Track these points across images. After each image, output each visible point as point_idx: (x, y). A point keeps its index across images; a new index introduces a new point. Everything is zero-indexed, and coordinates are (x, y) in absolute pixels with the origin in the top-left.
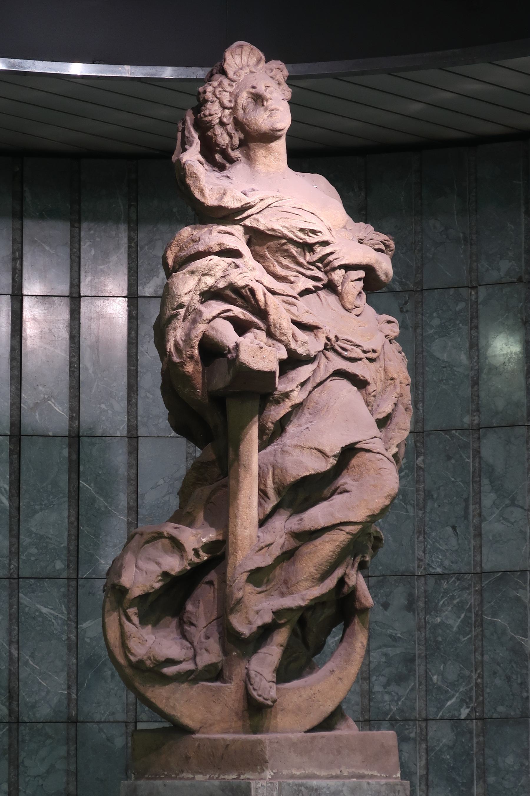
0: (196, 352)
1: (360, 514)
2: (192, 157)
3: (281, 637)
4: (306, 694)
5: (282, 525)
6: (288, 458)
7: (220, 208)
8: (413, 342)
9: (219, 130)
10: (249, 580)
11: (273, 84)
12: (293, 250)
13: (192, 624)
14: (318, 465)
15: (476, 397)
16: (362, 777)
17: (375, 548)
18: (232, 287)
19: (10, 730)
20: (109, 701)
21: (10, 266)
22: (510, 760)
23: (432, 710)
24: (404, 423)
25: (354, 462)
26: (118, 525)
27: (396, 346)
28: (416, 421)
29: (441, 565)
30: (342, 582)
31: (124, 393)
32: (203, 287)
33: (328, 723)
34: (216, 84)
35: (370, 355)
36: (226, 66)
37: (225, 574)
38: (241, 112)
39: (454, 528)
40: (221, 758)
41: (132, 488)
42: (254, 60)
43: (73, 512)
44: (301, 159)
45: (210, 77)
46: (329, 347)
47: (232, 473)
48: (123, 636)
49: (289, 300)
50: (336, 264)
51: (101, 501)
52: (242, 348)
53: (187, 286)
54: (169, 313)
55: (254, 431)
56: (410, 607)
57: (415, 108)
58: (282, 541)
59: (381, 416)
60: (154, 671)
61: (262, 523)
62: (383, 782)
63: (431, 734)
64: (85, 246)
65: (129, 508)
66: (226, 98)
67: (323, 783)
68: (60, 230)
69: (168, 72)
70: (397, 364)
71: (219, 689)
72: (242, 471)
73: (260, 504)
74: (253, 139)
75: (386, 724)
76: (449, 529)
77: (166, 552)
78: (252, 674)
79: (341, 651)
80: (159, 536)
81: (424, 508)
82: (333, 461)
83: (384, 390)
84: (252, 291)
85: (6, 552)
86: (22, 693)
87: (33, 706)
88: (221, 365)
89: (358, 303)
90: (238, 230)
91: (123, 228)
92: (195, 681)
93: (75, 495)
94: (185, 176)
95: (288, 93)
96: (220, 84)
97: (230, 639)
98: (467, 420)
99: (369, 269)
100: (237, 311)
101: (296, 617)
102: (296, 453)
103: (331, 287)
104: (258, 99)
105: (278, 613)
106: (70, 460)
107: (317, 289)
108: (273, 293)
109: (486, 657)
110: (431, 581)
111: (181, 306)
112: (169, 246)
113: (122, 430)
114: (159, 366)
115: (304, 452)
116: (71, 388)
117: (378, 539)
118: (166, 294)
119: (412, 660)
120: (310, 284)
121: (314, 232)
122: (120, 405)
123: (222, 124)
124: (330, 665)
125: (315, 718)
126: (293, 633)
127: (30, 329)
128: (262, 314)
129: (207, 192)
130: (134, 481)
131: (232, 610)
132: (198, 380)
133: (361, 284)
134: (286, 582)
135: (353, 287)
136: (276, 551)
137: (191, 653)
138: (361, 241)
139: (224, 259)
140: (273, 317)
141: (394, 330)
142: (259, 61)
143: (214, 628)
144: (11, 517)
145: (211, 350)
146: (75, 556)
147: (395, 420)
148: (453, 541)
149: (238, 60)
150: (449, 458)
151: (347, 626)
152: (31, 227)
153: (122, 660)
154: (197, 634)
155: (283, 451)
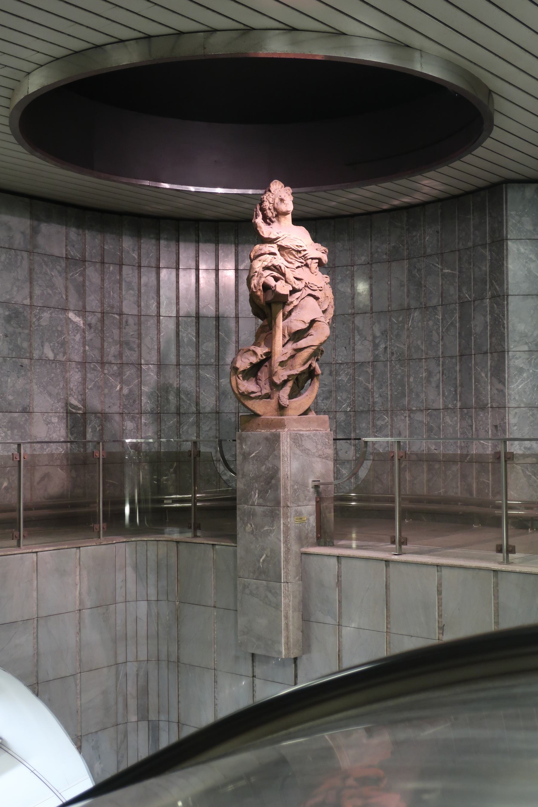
0: (261, 288)
1: (317, 343)
2: (259, 221)
3: (290, 384)
4: (299, 403)
5: (291, 346)
6: (292, 324)
7: (269, 238)
8: (333, 284)
9: (268, 211)
10: (279, 365)
11: (287, 195)
12: (294, 253)
13: (260, 380)
14: (304, 326)
15: (353, 303)
16: (317, 430)
17: (321, 354)
18: (273, 266)
19: (197, 416)
20: (230, 406)
21: (195, 259)
22: (364, 425)
23: (338, 409)
24: (331, 312)
25: (315, 325)
26: (232, 347)
27: (329, 286)
28: (335, 311)
29: (341, 360)
30: (310, 365)
31: (234, 302)
32: (264, 266)
33: (305, 413)
34: (267, 195)
35: (320, 289)
36: (271, 189)
37: (271, 363)
38: (276, 205)
39: (345, 348)
40: (270, 424)
41: (237, 335)
42: (280, 187)
43: (217, 343)
44: (296, 221)
45: (265, 193)
46: (306, 286)
47: (273, 329)
48: (237, 384)
49: (293, 270)
50: (309, 257)
51: (227, 339)
52: (277, 286)
53: (258, 265)
54: (252, 274)
55: (281, 315)
56: (331, 374)
57: (334, 204)
58: (290, 352)
59: (324, 310)
60: (248, 396)
61: (283, 346)
62: (324, 432)
63: (337, 416)
64: (220, 252)
65: (236, 341)
66: (271, 200)
67: (304, 433)
68: (211, 247)
69: (250, 192)
70: (329, 291)
71: (269, 401)
72: (277, 328)
73: (283, 339)
74: (279, 214)
75: (322, 413)
76: (344, 348)
77: (251, 356)
78: (281, 396)
79: (310, 388)
80: (249, 350)
81: (335, 341)
82: (308, 325)
83: (325, 300)
84: (280, 267)
85: (195, 356)
86: (201, 404)
87: (204, 408)
88: (270, 292)
89: (316, 271)
90: (275, 246)
91: (233, 246)
92: (261, 399)
93: (218, 337)
94: (257, 227)
95: (292, 198)
96: (269, 195)
97: (273, 385)
98: (350, 311)
99: (320, 259)
100: (275, 274)
101: (295, 378)
102: (295, 322)
103: (307, 265)
104: (282, 200)
105: (289, 376)
106: (216, 325)
107: (302, 266)
108: (287, 267)
109: (356, 391)
110: (338, 365)
111: (256, 272)
112: (251, 251)
113: (233, 315)
114: (248, 293)
115: (297, 322)
116: (216, 301)
117: (322, 351)
118: (251, 268)
119: (331, 392)
120: (300, 264)
121: (301, 246)
122: (233, 306)
123: (269, 209)
124: (306, 393)
125: (302, 411)
126: (294, 383)
127: (202, 281)
128: (284, 275)
129: (265, 233)
130: (237, 332)
131: (274, 375)
132: (262, 297)
133: (317, 264)
134: (292, 366)
135: (314, 265)
136: (288, 355)
137: (260, 389)
138: (317, 250)
139: (268, 257)
140: (287, 276)
141: (328, 280)
142: (282, 187)
143: (268, 381)
144: (196, 345)
145: (266, 287)
146: (218, 358)
147: (328, 311)
148: (345, 352)
149: (275, 186)
150: (344, 324)
151: (312, 380)
152: (202, 246)
153: (237, 392)
154: (262, 383)
155: (291, 322)
